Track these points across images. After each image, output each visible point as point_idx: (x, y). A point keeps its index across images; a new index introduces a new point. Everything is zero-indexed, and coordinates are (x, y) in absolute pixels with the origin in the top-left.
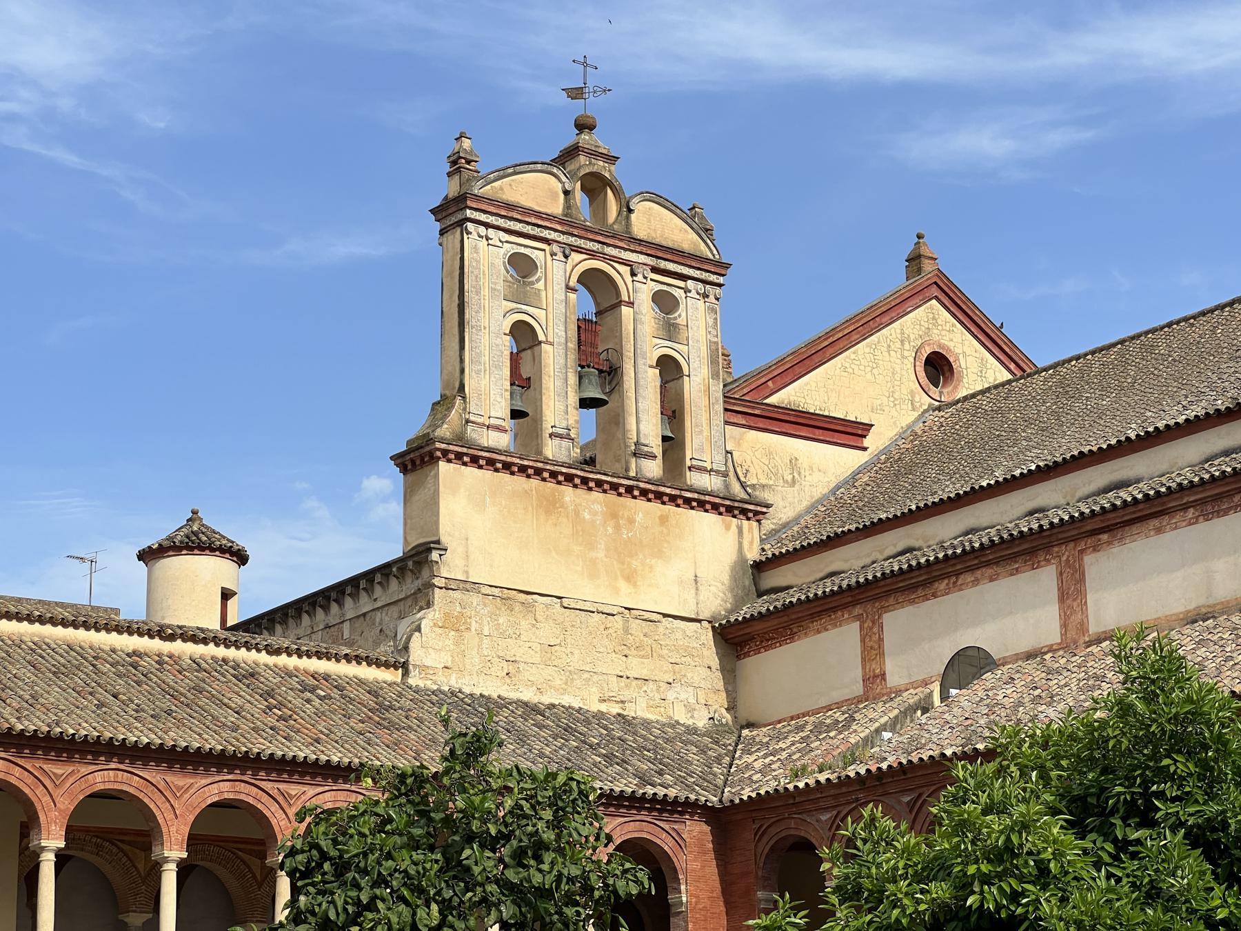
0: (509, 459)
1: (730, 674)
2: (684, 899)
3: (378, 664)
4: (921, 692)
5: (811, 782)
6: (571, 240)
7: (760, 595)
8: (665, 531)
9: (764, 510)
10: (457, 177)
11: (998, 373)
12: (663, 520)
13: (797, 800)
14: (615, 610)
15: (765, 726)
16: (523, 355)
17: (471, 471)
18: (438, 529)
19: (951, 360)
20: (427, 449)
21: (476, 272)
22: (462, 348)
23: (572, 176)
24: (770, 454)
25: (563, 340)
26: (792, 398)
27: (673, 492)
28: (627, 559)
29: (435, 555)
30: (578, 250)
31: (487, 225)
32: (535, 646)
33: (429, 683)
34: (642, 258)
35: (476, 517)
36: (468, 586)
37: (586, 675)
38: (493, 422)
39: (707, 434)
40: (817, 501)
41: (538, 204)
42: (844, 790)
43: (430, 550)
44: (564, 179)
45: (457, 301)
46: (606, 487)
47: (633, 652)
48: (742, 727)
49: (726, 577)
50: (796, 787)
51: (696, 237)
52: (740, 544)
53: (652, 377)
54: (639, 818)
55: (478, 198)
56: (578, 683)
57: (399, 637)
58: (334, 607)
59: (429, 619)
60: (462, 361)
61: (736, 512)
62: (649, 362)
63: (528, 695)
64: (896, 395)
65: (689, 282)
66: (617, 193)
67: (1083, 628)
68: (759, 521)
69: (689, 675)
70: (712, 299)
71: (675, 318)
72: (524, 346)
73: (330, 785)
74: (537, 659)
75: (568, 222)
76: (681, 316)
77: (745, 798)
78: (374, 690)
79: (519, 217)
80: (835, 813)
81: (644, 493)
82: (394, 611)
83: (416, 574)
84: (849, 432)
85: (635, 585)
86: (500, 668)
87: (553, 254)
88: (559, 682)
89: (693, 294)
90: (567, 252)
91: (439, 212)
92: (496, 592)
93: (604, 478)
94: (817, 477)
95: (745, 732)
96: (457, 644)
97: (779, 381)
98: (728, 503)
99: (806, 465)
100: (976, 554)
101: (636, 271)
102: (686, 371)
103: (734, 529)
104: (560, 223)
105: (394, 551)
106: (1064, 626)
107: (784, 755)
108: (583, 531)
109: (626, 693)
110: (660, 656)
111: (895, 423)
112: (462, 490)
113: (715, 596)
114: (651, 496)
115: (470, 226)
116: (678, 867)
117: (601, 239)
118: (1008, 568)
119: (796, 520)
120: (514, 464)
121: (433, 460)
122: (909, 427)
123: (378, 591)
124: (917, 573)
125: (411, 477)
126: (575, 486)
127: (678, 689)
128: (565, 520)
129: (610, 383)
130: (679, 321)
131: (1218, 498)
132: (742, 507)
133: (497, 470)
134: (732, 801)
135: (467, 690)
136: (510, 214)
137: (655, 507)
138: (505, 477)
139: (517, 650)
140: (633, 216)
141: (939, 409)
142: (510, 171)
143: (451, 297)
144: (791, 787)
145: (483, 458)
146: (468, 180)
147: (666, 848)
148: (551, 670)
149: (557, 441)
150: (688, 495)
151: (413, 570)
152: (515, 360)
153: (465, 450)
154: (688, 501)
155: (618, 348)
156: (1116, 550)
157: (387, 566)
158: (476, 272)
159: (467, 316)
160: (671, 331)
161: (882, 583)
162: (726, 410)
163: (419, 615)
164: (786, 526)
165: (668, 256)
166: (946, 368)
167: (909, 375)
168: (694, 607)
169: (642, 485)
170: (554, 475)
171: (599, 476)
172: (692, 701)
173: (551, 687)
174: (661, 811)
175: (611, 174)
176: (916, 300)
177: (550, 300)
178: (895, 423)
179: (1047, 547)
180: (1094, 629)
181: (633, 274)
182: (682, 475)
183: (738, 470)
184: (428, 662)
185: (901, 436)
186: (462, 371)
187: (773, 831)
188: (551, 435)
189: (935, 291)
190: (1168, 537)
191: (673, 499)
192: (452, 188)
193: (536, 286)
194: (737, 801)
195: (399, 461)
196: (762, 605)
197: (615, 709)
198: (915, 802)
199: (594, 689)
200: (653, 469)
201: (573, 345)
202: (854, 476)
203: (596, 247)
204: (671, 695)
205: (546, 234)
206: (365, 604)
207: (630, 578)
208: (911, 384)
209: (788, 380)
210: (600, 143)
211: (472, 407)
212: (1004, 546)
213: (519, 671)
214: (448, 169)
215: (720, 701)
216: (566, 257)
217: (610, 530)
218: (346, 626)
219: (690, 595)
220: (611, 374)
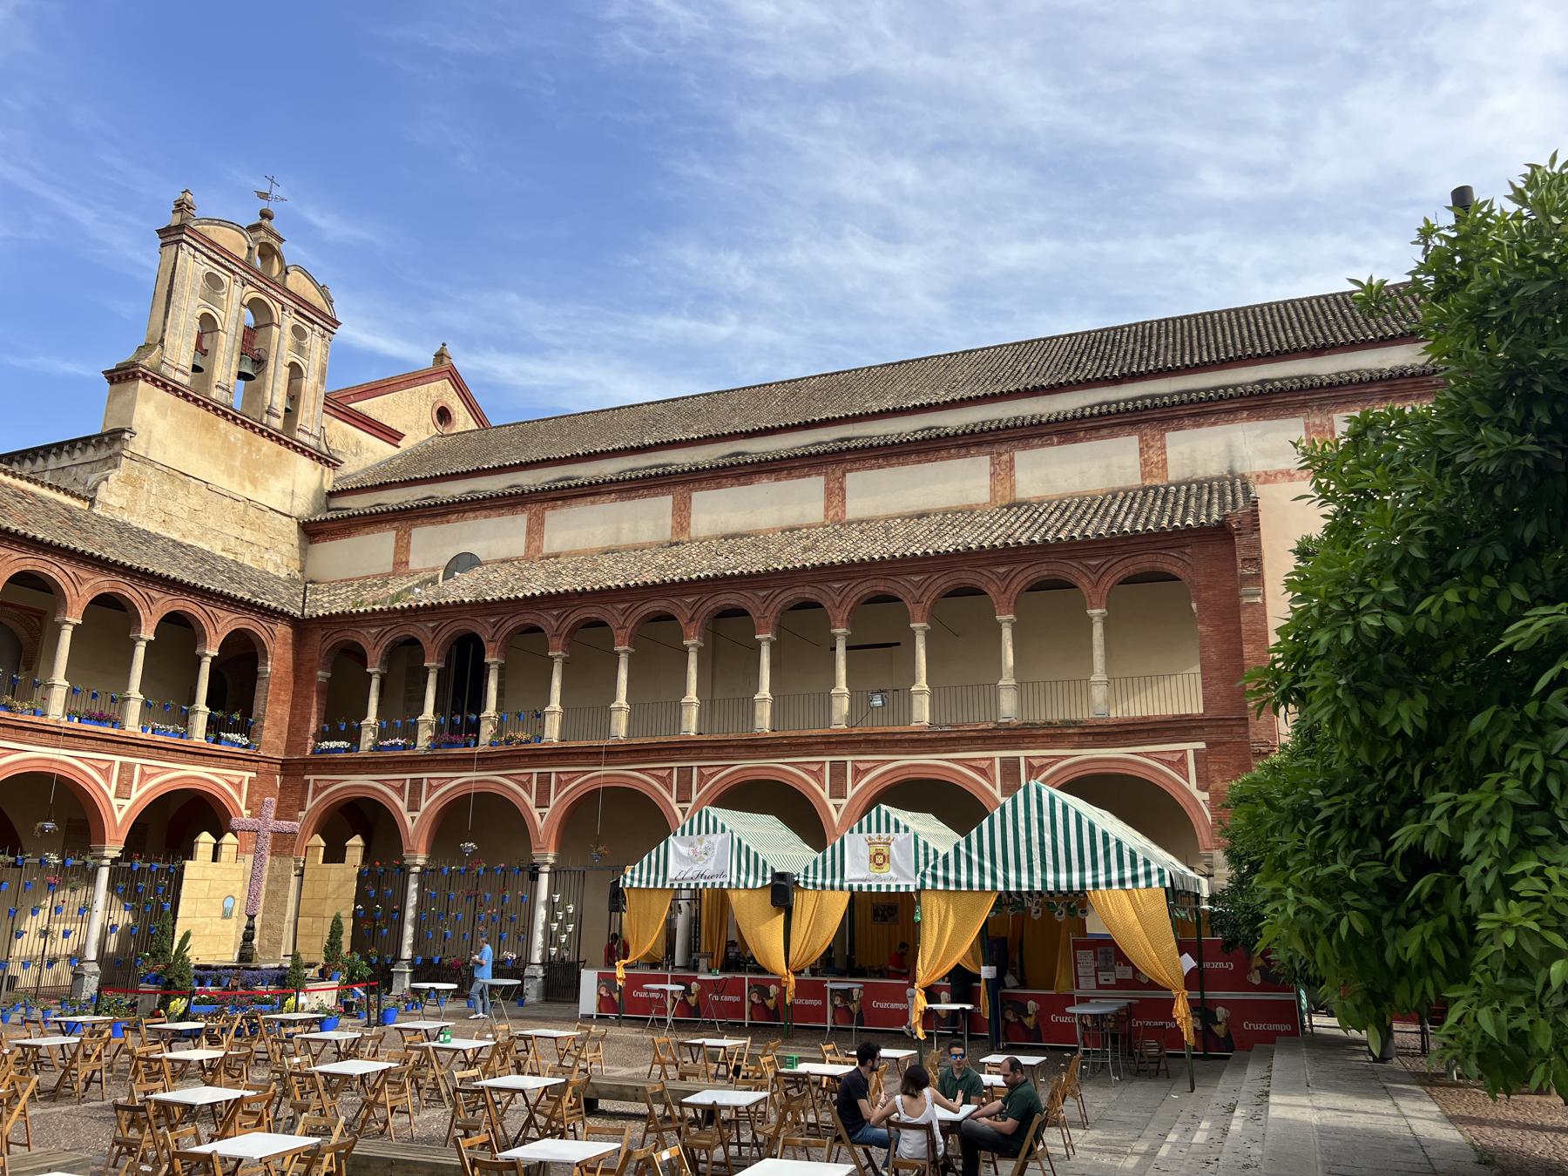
1: (304, 551)
3: (73, 495)
7: (329, 510)
11: (472, 425)
12: (279, 454)
17: (160, 392)
22: (166, 316)
23: (255, 240)
24: (345, 435)
27: (286, 439)
29: (127, 436)
30: (252, 284)
35: (155, 419)
39: (311, 416)
43: (123, 431)
49: (310, 496)
53: (285, 372)
55: (193, 230)
58: (40, 461)
59: (114, 475)
63: (176, 536)
66: (281, 260)
67: (539, 550)
73: (32, 554)
74: (185, 516)
75: (248, 265)
76: (307, 343)
81: (270, 435)
82: (88, 468)
84: (393, 436)
86: (158, 516)
106: (528, 547)
113: (303, 506)
119: (355, 475)
121: (135, 377)
123: (77, 454)
131: (631, 490)
132: (326, 460)
137: (275, 445)
138: (183, 402)
139: (173, 508)
151: (112, 440)
152: (200, 337)
154: (295, 447)
156: (565, 510)
157: (89, 438)
160: (300, 349)
167: (428, 416)
170: (215, 409)
179: (524, 504)
180: (545, 550)
184: (110, 501)
190: (598, 507)
191: (287, 443)
192: (175, 220)
197: (231, 557)
200: (277, 423)
201: (239, 338)
202: (391, 460)
204: (266, 556)
206: (65, 461)
207: (254, 482)
219: (288, 501)
220: (260, 363)
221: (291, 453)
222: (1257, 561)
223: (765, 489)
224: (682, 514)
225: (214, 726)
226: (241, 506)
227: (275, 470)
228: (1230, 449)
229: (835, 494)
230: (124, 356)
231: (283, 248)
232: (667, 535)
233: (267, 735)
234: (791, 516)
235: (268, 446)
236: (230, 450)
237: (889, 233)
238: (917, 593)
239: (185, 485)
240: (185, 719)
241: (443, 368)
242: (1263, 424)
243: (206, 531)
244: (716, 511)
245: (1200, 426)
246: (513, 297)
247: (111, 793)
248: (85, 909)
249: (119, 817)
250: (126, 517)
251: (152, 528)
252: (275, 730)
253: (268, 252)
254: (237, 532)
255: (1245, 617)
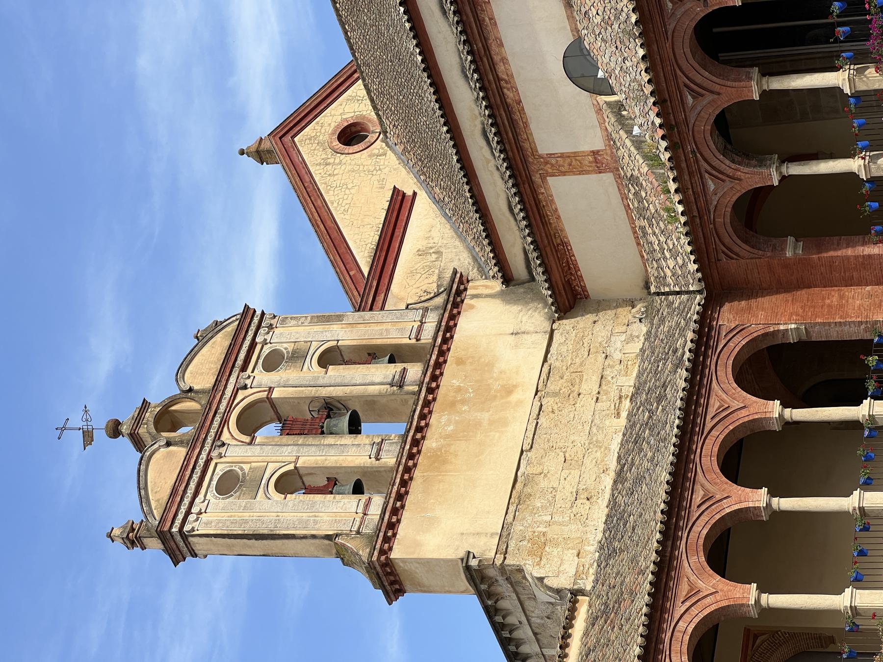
0: (393, 495)
1: (601, 305)
2: (793, 326)
4: (607, 112)
5: (677, 198)
6: (210, 440)
7: (532, 279)
8: (470, 360)
9: (458, 275)
10: (145, 541)
11: (358, 89)
12: (460, 362)
13: (696, 213)
14: (537, 404)
15: (647, 271)
16: (307, 484)
17: (402, 530)
18: (451, 560)
19: (346, 124)
20: (378, 568)
21: (228, 523)
23: (155, 439)
24: (412, 273)
25: (295, 448)
26: (366, 255)
27: (436, 355)
28: (492, 393)
29: (473, 563)
30: (219, 434)
31: (188, 513)
32: (564, 475)
33: (592, 571)
34: (232, 380)
35: (443, 528)
36: (505, 534)
37: (594, 430)
38: (360, 510)
39: (391, 326)
40: (456, 233)
41: (176, 469)
42: (684, 165)
43: (468, 568)
44: (156, 446)
45: (253, 541)
46: (426, 411)
47: (576, 388)
48: (649, 293)
49: (515, 308)
50: (683, 214)
51: (220, 335)
52: (487, 296)
53: (335, 372)
54: (713, 367)
55: (162, 520)
56: (600, 437)
57: (553, 600)
59: (533, 570)
60: (305, 537)
61: (459, 299)
62: (323, 374)
63: (608, 481)
64: (371, 168)
65: (257, 340)
66: (174, 401)
68: (468, 281)
69: (600, 340)
70: (274, 322)
71: (288, 352)
72: (301, 484)
74: (576, 473)
75: (193, 444)
76: (286, 348)
77: (696, 267)
78: (593, 621)
79: (184, 485)
80: (707, 175)
82: (529, 604)
83: (492, 582)
84: (399, 207)
85: (515, 386)
86: (582, 507)
87: (220, 456)
88: (598, 454)
89: (268, 337)
90: (219, 443)
91: (176, 557)
92: (512, 508)
93: (417, 412)
94: (436, 234)
95: (653, 289)
96: (557, 545)
97: (351, 265)
98: (449, 306)
99: (425, 243)
100: (478, 59)
101: (242, 384)
102: (334, 343)
103: (473, 302)
104: (193, 449)
105: (473, 603)
107: (662, 239)
108: (464, 431)
109: (612, 394)
110: (581, 365)
111: (395, 169)
112: (418, 538)
113: (533, 318)
114: (438, 372)
115: (187, 528)
116: (762, 332)
117: (211, 415)
118: (490, 28)
119: (471, 250)
120: (398, 492)
122: (399, 158)
123: (511, 620)
124: (499, 119)
125: (407, 585)
126: (423, 438)
127: (612, 349)
128: (453, 447)
129: (339, 409)
130: (290, 349)
132: (455, 294)
133: (403, 507)
134: (699, 280)
135: (600, 536)
136: (180, 492)
137: (448, 369)
138: (410, 500)
139: (567, 490)
140: (196, 387)
141: (385, 133)
142: (143, 492)
143: (250, 547)
144: (683, 219)
145: (390, 518)
146: (148, 530)
147: (743, 343)
148: (587, 461)
149: (383, 454)
150: (439, 340)
151: (487, 582)
152: (310, 490)
153: (381, 534)
154: (445, 341)
155: (308, 402)
157: (487, 609)
158: (228, 523)
159: (266, 532)
160: (298, 356)
161: (510, 153)
162: (371, 309)
163: (530, 580)
164: (475, 259)
165: (233, 358)
166: (354, 129)
168: (539, 336)
169: (427, 379)
170: (411, 456)
171: (416, 417)
172: (623, 337)
173: (602, 461)
174: (707, 346)
175: (158, 406)
176: (294, 154)
177: (260, 459)
178: (395, 169)
181: (245, 387)
182: (423, 347)
183: (423, 299)
184: (572, 571)
185: (406, 164)
186: (314, 537)
187: (727, 240)
188: (377, 459)
189: (287, 139)
192: (154, 545)
193: (247, 471)
194: (699, 275)
195: (392, 596)
196: (540, 278)
197: (626, 404)
198: (693, 90)
199: (607, 422)
200: (414, 371)
201: (301, 440)
202: (437, 202)
203: (218, 418)
205: (201, 462)
206: (525, 633)
207: (509, 390)
208: (363, 157)
209: (350, 258)
210: (131, 416)
211: (346, 528)
212: (469, 31)
213: (586, 490)
214: (139, 549)
215: (625, 314)
216: (223, 444)
217: (465, 408)
218: (547, 652)
219: (529, 339)
220: (330, 408)
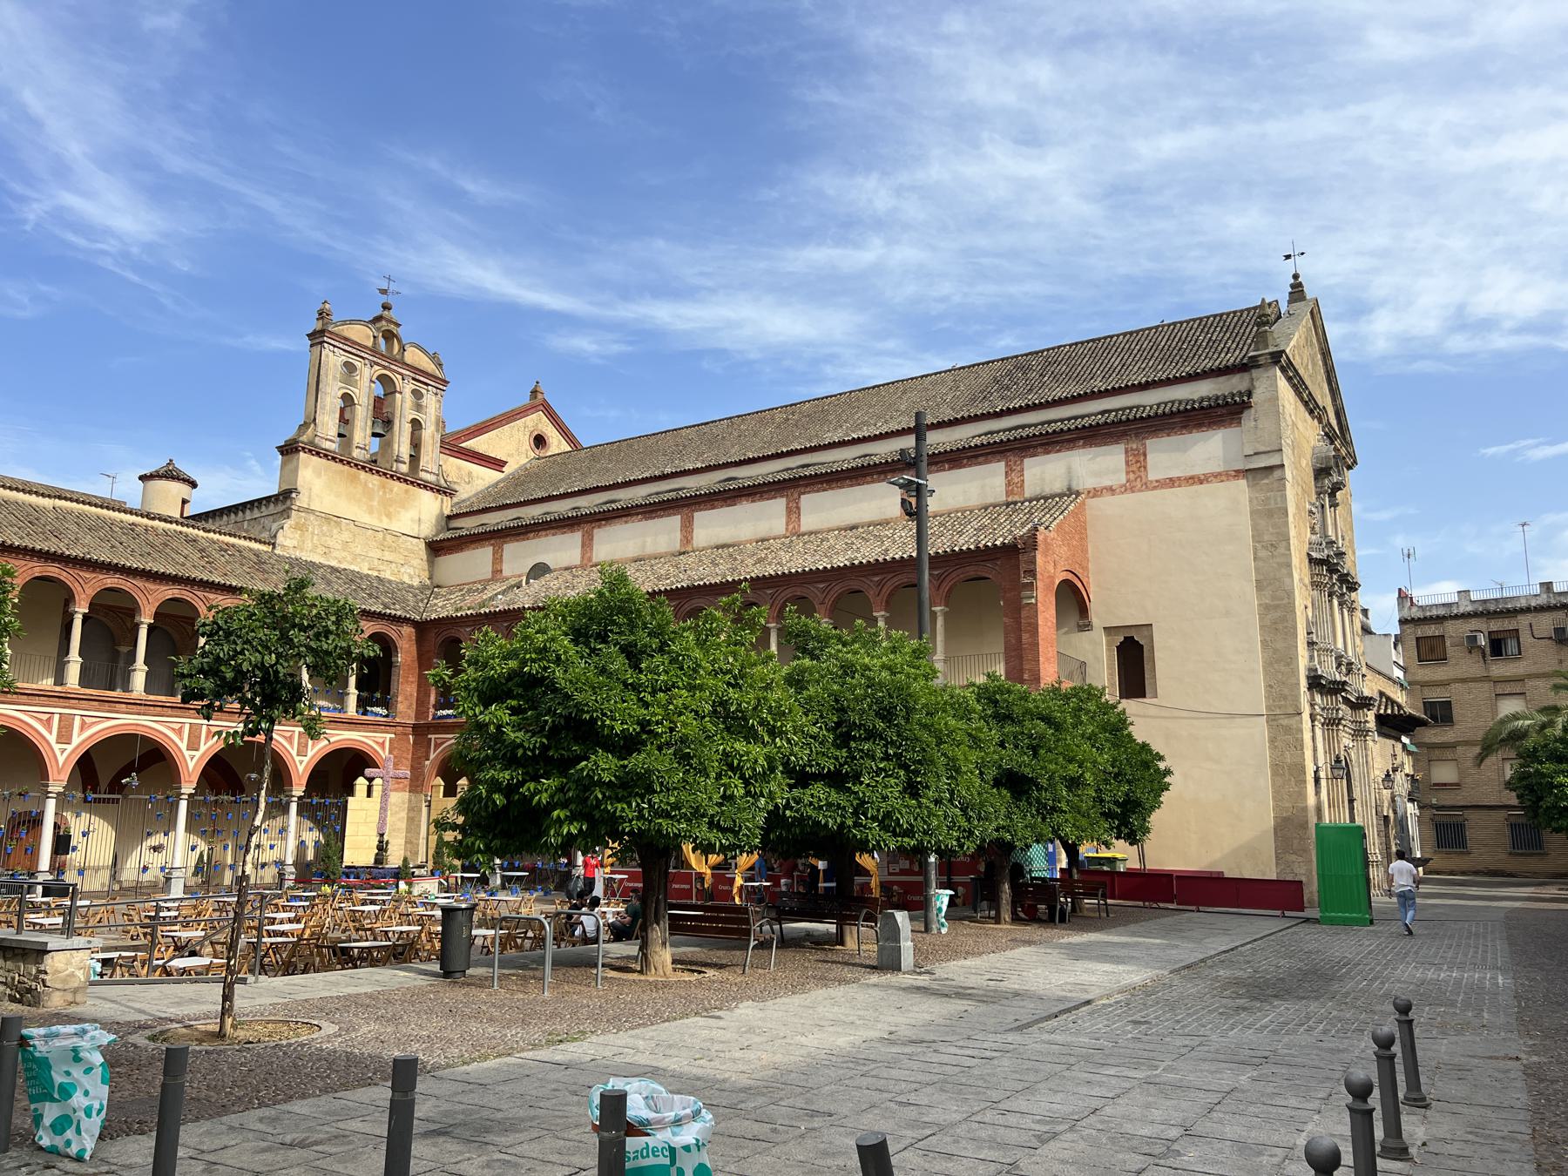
1: (431, 563)
12: (407, 491)
17: (315, 458)
23: (378, 329)
24: (459, 468)
27: (412, 479)
35: (316, 481)
39: (432, 460)
53: (408, 428)
59: (288, 524)
63: (334, 563)
66: (399, 341)
67: (590, 559)
75: (374, 351)
76: (424, 401)
84: (498, 464)
86: (320, 550)
113: (428, 529)
121: (297, 451)
137: (403, 485)
139: (330, 543)
152: (342, 410)
160: (418, 407)
167: (526, 443)
179: (579, 524)
192: (318, 326)
200: (404, 468)
206: (256, 514)
207: (389, 515)
220: (388, 423)
221: (416, 489)
222: (1032, 573)
223: (745, 508)
224: (687, 527)
225: (363, 704)
226: (380, 535)
227: (404, 504)
228: (1069, 470)
229: (793, 512)
230: (289, 434)
231: (400, 331)
232: (677, 547)
233: (400, 707)
234: (762, 529)
235: (398, 487)
236: (369, 493)
237: (1030, 137)
238: (822, 597)
239: (338, 524)
240: (341, 699)
241: (538, 402)
242: (1094, 449)
243: (355, 556)
244: (712, 526)
245: (1048, 453)
246: (660, 244)
247: (294, 753)
248: (283, 830)
249: (301, 768)
250: (298, 554)
251: (317, 559)
252: (406, 703)
253: (389, 336)
254: (378, 554)
255: (1024, 613)
